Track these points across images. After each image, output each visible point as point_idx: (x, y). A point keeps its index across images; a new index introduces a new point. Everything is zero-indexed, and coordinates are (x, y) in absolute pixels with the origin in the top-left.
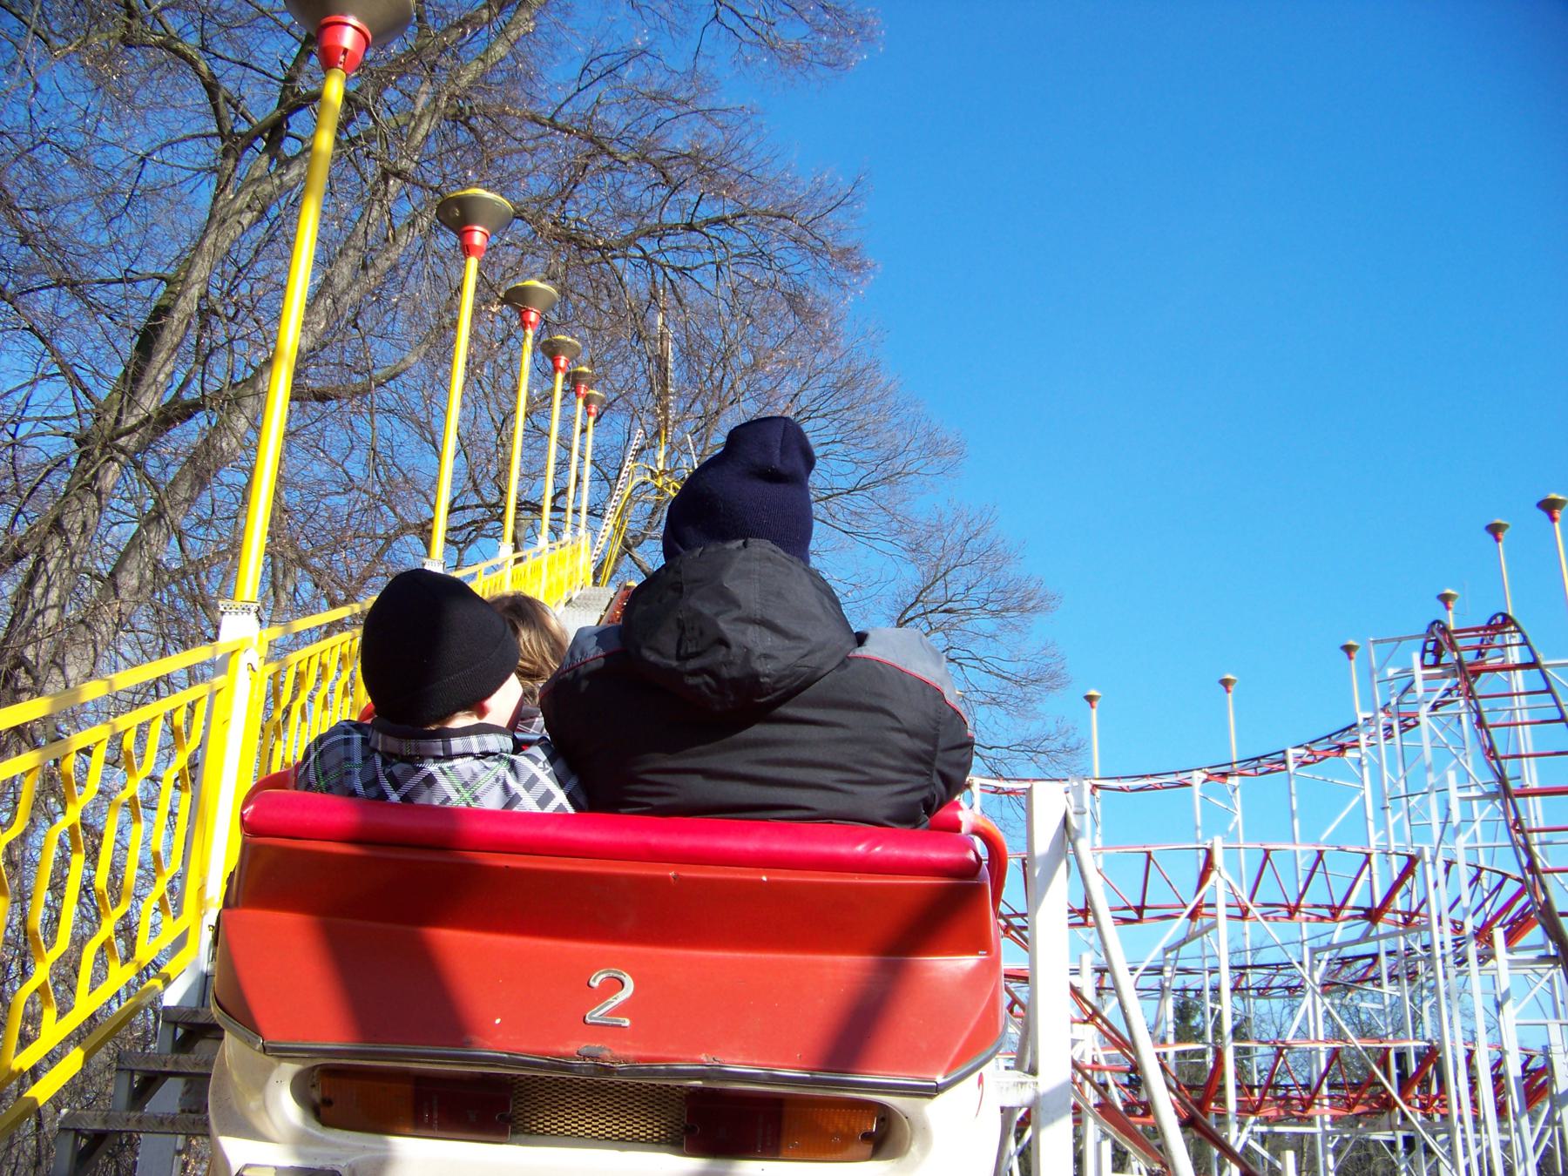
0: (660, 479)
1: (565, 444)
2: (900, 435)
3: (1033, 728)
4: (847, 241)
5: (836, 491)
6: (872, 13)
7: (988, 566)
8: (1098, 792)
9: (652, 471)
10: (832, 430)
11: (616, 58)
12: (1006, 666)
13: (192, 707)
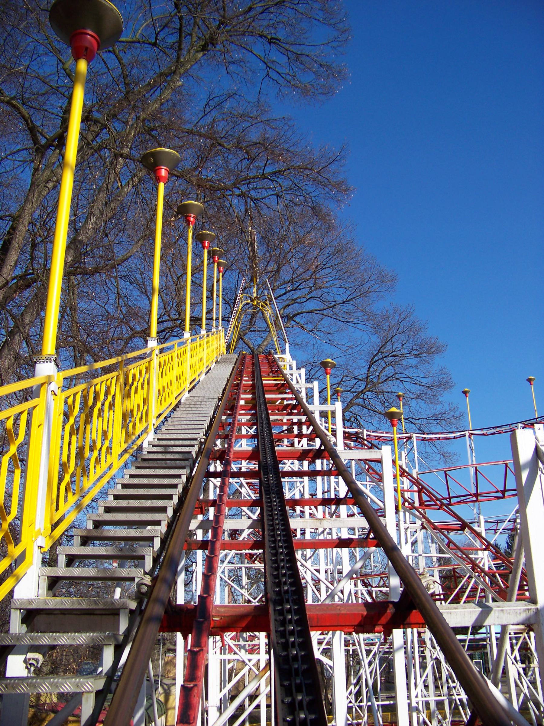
0: (255, 301)
1: (210, 291)
2: (365, 274)
3: (439, 408)
4: (341, 178)
5: (337, 303)
6: (344, 66)
7: (412, 333)
8: (472, 437)
9: (250, 298)
10: (333, 273)
11: (221, 98)
12: (423, 380)
13: (17, 417)
